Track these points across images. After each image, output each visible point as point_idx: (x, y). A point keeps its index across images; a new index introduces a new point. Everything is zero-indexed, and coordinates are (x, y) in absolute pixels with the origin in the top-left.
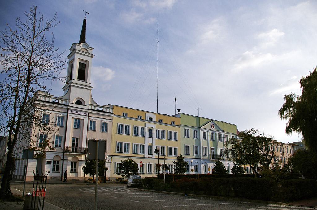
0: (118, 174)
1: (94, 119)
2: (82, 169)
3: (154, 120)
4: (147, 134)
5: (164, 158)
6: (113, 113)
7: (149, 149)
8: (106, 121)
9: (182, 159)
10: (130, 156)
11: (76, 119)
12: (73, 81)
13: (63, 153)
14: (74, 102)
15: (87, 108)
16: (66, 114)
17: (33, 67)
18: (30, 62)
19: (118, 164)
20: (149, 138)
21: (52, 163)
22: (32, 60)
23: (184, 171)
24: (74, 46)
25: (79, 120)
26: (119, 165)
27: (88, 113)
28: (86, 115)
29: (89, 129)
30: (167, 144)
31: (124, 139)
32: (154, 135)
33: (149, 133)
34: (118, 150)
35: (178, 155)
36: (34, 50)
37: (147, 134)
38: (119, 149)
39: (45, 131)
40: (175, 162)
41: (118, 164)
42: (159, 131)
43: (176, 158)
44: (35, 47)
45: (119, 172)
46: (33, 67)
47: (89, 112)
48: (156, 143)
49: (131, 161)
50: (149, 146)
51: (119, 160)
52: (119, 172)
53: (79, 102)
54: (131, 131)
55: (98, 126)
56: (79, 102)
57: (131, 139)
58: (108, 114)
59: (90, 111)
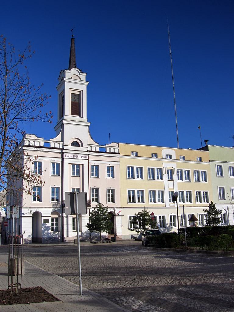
0: (132, 230)
1: (96, 163)
2: (86, 226)
3: (174, 157)
4: (165, 176)
5: (183, 206)
6: (119, 153)
7: (197, 196)
8: (112, 164)
9: (214, 206)
10: (145, 207)
11: (74, 165)
12: (65, 117)
13: (183, 208)
14: (70, 144)
15: (86, 149)
16: (61, 160)
17: (8, 110)
18: (4, 104)
19: (130, 217)
20: (169, 181)
21: (50, 221)
22: (6, 102)
23: (218, 221)
24: (63, 73)
25: (78, 165)
26: (132, 218)
27: (87, 156)
28: (85, 159)
29: (91, 176)
30: (193, 186)
31: (137, 184)
32: (175, 177)
33: (168, 175)
34: (130, 200)
35: (210, 202)
36: (7, 89)
37: (165, 176)
38: (131, 197)
39: (28, 183)
40: (205, 211)
41: (130, 217)
42: (181, 171)
43: (208, 205)
44: (9, 85)
45: (132, 228)
46: (8, 110)
47: (89, 155)
48: (176, 186)
49: (145, 214)
50: (169, 192)
51: (134, 212)
52: (132, 228)
53: (75, 144)
54: (145, 173)
55: (103, 171)
56: (75, 144)
57: (145, 185)
58: (97, 153)
59: (90, 153)
